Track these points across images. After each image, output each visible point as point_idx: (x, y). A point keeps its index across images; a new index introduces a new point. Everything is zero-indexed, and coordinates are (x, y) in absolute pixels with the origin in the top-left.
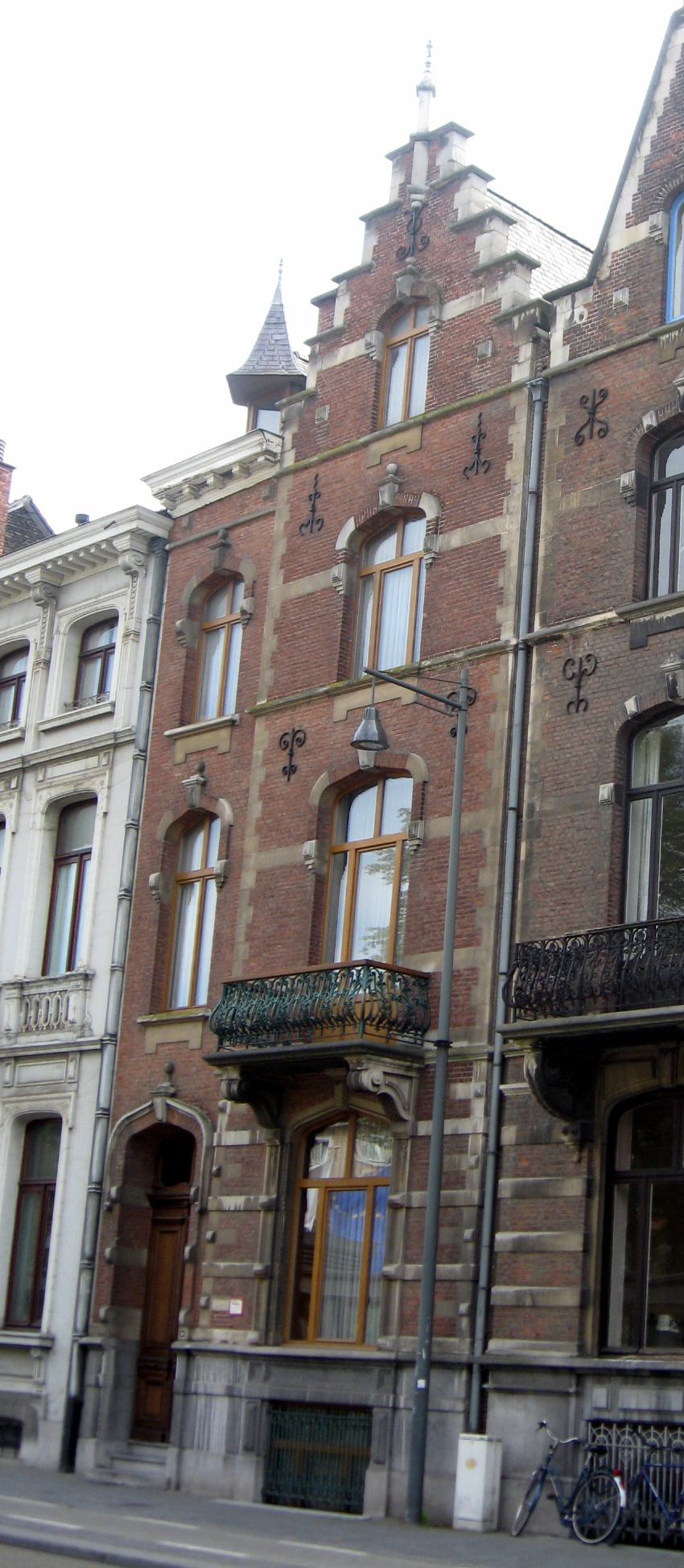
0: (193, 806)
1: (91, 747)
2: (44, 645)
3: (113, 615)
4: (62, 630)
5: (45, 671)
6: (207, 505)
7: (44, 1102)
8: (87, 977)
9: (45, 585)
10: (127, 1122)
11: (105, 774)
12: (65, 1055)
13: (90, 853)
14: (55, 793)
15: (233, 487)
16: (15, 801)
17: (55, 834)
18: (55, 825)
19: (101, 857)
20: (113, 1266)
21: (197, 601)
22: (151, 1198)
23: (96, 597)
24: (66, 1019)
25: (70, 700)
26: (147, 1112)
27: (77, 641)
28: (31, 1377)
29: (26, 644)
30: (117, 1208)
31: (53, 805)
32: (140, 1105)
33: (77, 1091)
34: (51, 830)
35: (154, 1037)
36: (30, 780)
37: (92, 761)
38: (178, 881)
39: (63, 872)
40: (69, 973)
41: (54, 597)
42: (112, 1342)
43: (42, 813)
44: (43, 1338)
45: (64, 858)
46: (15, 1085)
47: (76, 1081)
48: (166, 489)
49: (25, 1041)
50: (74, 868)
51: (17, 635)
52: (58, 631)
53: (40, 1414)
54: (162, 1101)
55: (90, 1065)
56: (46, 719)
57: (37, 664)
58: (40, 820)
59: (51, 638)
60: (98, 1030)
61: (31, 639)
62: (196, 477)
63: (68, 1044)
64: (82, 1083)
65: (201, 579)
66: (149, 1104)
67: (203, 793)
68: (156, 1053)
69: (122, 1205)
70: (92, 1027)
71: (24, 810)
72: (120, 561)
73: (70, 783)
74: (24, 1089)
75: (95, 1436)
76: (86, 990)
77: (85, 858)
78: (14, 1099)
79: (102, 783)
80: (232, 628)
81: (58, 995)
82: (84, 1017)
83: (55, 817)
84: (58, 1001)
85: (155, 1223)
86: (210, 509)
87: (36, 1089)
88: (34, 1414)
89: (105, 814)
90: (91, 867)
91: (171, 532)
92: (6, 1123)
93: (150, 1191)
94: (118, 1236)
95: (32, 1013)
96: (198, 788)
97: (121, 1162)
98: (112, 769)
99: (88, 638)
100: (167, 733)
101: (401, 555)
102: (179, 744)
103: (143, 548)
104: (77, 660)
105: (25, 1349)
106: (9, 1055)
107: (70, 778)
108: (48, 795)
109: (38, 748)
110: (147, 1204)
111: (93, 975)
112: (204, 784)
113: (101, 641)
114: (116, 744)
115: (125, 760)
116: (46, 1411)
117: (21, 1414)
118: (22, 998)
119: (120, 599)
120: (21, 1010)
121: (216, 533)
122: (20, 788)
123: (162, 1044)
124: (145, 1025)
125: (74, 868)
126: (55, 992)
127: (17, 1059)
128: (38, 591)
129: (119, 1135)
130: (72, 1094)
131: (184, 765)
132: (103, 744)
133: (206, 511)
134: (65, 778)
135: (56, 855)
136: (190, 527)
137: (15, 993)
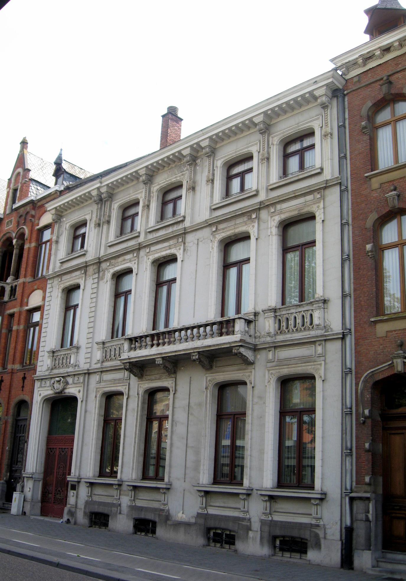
0: (395, 207)
1: (309, 190)
2: (147, 199)
3: (136, 201)
4: (275, 143)
5: (148, 210)
6: (380, 64)
7: (300, 368)
8: (78, 348)
9: (264, 123)
10: (370, 374)
11: (320, 202)
12: (314, 342)
13: (131, 291)
14: (283, 216)
15: (389, 57)
16: (256, 225)
17: (282, 238)
18: (281, 234)
19: (82, 305)
20: (370, 453)
21: (370, 113)
22: (381, 415)
23: (298, 124)
24: (70, 363)
25: (282, 175)
26: (387, 367)
27: (73, 232)
28: (311, 515)
29: (138, 201)
30: (369, 421)
31: (154, 262)
32: (378, 366)
33: (325, 361)
34: (280, 235)
35: (382, 329)
36: (142, 253)
37: (310, 198)
38: (380, 249)
39: (68, 313)
40: (71, 347)
41: (110, 197)
42: (374, 495)
43: (276, 227)
44: (118, 481)
45: (69, 308)
46: (276, 360)
47: (323, 355)
48: (347, 63)
49: (280, 338)
50: (72, 311)
51: (245, 151)
52: (273, 144)
53: (321, 535)
54: (401, 361)
55: (334, 347)
56: (150, 226)
57: (144, 207)
58: (275, 231)
59: (269, 147)
60: (337, 327)
61: (88, 219)
62: (368, 53)
63: (317, 337)
64: (327, 357)
65: (374, 102)
66: (390, 362)
67: (398, 200)
68: (386, 337)
69: (372, 420)
70: (331, 327)
71: (261, 228)
72: (319, 101)
73: (295, 210)
74: (281, 363)
75: (370, 550)
76: (324, 308)
77: (76, 307)
78: (277, 367)
79: (318, 207)
80: (396, 123)
81: (115, 347)
82: (325, 322)
83: (281, 229)
84: (111, 350)
85: (384, 429)
86: (372, 70)
87: (293, 362)
88: (317, 536)
89: (137, 274)
90: (78, 311)
91: (344, 86)
92: (272, 381)
93: (380, 412)
94: (372, 436)
95: (57, 362)
96: (396, 197)
97: (368, 396)
98: (324, 199)
99: (230, 169)
100: (366, 175)
101: (394, 116)
102: (374, 180)
103: (330, 94)
104: (161, 205)
105: (157, 489)
106: (271, 345)
107: (294, 208)
108: (152, 257)
109: (211, 216)
110: (379, 419)
111: (328, 301)
112: (399, 196)
113: (131, 212)
114: (327, 186)
115: (334, 195)
116: (325, 534)
117: (306, 535)
118: (276, 317)
119: (314, 122)
120: (275, 323)
121: (382, 79)
122: (258, 218)
123: (391, 331)
124: (375, 322)
125: (72, 311)
126: (65, 354)
127: (275, 347)
128: (207, 149)
129: (365, 381)
130: (323, 362)
131: (380, 190)
132: (135, 248)
133: (369, 72)
134: (69, 281)
135: (66, 306)
136: (359, 81)
137: (272, 314)
